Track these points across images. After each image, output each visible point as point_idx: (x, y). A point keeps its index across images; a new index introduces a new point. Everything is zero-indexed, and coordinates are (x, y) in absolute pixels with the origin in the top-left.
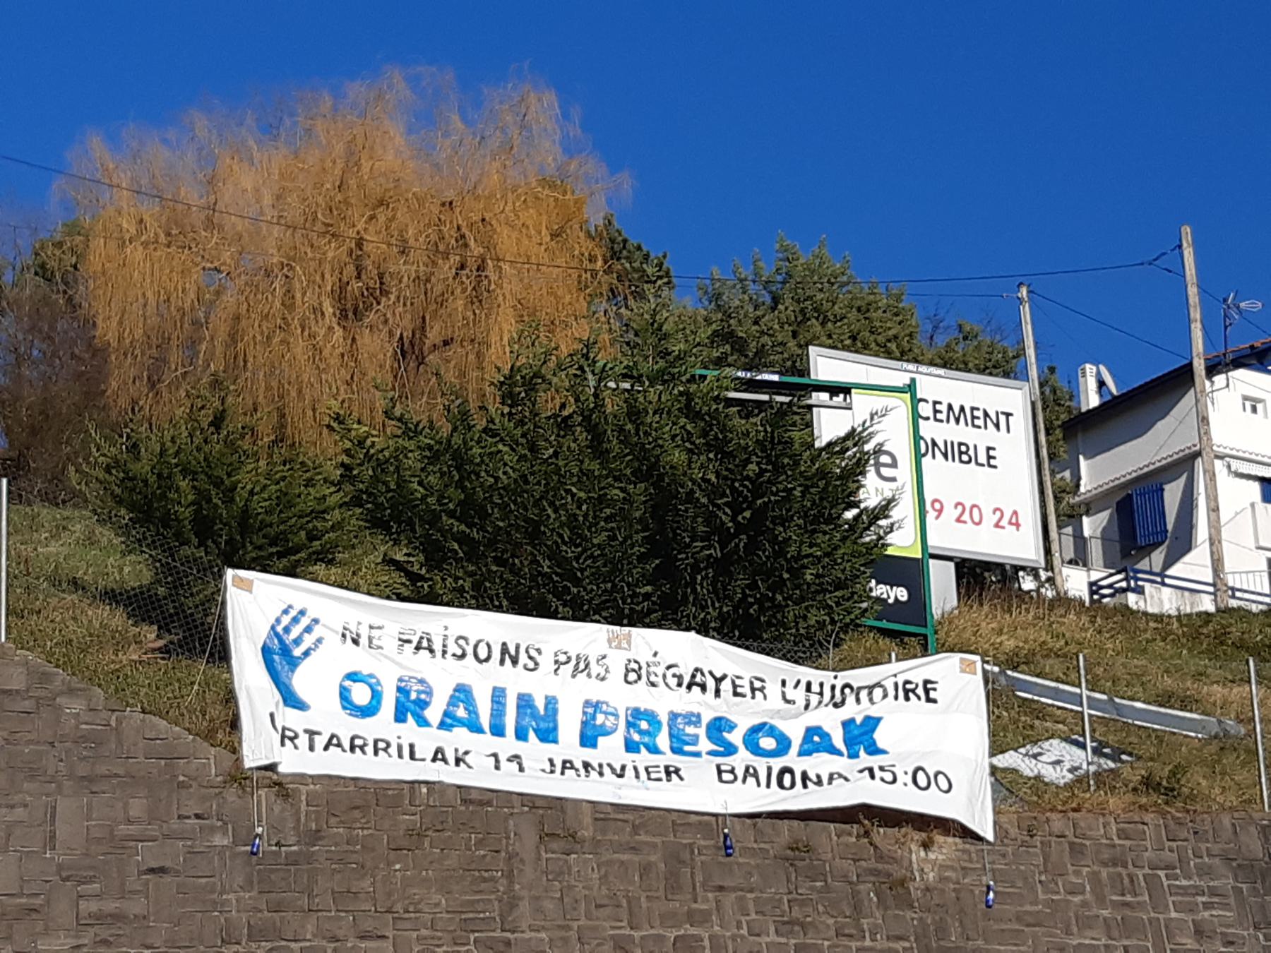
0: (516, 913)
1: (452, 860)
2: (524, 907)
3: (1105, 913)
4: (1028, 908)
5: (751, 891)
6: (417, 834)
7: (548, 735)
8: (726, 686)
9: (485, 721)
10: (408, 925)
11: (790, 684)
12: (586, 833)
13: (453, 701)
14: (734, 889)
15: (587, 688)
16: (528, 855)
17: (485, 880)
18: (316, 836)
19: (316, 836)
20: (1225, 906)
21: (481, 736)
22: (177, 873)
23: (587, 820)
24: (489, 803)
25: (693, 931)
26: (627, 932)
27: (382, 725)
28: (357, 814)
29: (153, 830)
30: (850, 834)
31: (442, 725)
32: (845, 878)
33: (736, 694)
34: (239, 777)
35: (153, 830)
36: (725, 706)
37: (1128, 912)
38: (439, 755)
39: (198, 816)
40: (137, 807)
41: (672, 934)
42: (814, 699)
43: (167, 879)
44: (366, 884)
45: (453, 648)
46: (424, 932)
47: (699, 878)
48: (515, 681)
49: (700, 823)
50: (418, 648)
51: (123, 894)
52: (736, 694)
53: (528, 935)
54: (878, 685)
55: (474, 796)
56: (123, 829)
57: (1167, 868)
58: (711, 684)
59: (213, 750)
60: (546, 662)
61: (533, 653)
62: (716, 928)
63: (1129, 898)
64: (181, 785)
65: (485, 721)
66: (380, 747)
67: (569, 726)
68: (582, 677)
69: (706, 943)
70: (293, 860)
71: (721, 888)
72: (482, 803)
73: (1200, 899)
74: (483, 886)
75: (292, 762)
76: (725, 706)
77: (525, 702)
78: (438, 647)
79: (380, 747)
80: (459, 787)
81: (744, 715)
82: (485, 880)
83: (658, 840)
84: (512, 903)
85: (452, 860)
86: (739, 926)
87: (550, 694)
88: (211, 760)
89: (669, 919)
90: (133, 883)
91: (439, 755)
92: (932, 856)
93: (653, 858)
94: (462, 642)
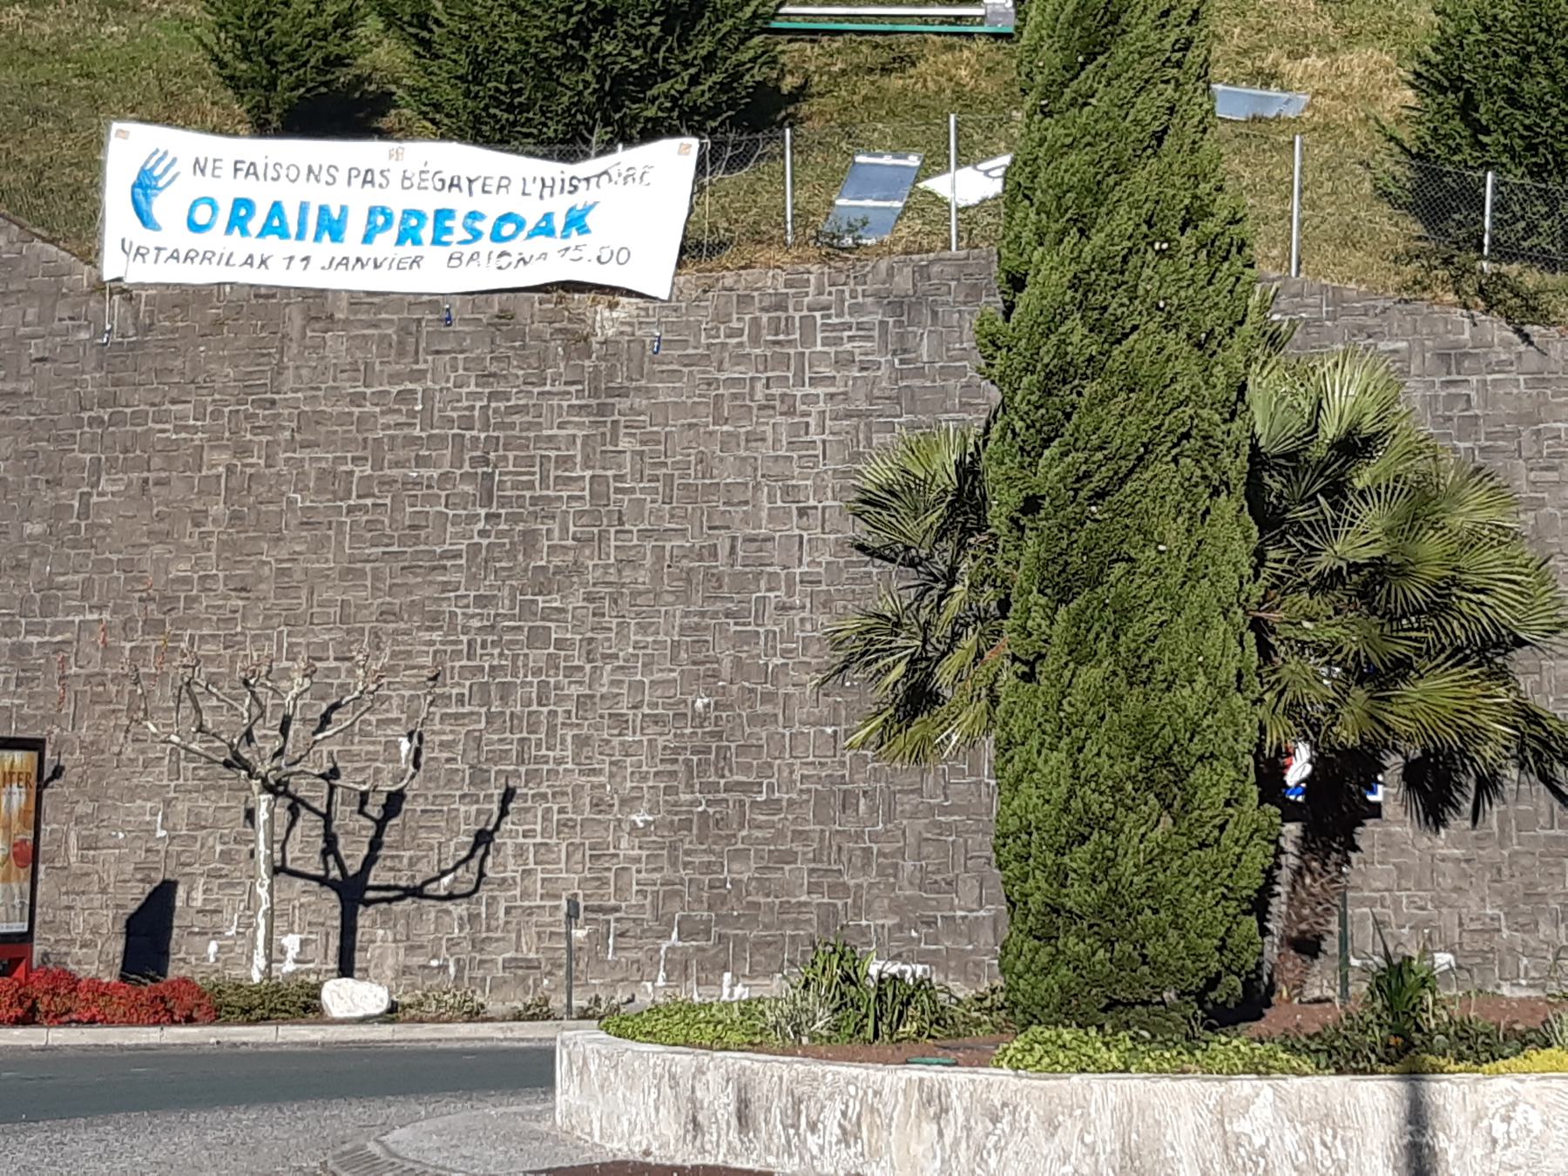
0: (282, 378)
1: (243, 340)
2: (290, 374)
3: (758, 351)
4: (690, 351)
5: (462, 352)
6: (218, 323)
7: (336, 237)
8: (477, 186)
9: (293, 229)
10: (205, 392)
11: (529, 181)
12: (339, 316)
13: (270, 217)
14: (448, 352)
15: (373, 196)
16: (295, 334)
17: (263, 355)
18: (150, 328)
19: (150, 328)
20: (869, 338)
21: (285, 242)
22: (55, 361)
23: (344, 304)
24: (274, 296)
25: (410, 386)
26: (362, 389)
27: (214, 239)
28: (177, 310)
29: (40, 330)
30: (549, 302)
31: (261, 235)
32: (540, 338)
33: (484, 191)
34: (99, 287)
35: (40, 330)
36: (479, 202)
37: (778, 349)
38: (249, 262)
39: (71, 319)
40: (31, 314)
41: (395, 389)
42: (547, 191)
43: (48, 366)
44: (178, 363)
45: (271, 173)
46: (217, 397)
47: (423, 345)
48: (317, 195)
49: (430, 302)
50: (247, 174)
51: (19, 377)
52: (484, 191)
53: (290, 395)
54: (606, 172)
55: (263, 291)
56: (22, 330)
57: (822, 309)
58: (464, 184)
59: (87, 268)
60: (342, 176)
61: (332, 171)
62: (429, 383)
63: (781, 337)
64: (64, 295)
65: (293, 229)
66: (207, 257)
67: (356, 226)
68: (368, 186)
69: (419, 396)
70: (133, 346)
71: (438, 352)
72: (267, 297)
73: (847, 334)
74: (262, 360)
75: (138, 273)
76: (479, 202)
77: (323, 210)
78: (260, 172)
79: (207, 257)
80: (252, 286)
81: (493, 207)
82: (263, 355)
83: (395, 317)
84: (280, 370)
85: (243, 340)
86: (447, 381)
87: (323, 203)
88: (84, 274)
89: (395, 378)
90: (26, 370)
91: (249, 262)
92: (615, 315)
93: (390, 331)
94: (332, 171)
